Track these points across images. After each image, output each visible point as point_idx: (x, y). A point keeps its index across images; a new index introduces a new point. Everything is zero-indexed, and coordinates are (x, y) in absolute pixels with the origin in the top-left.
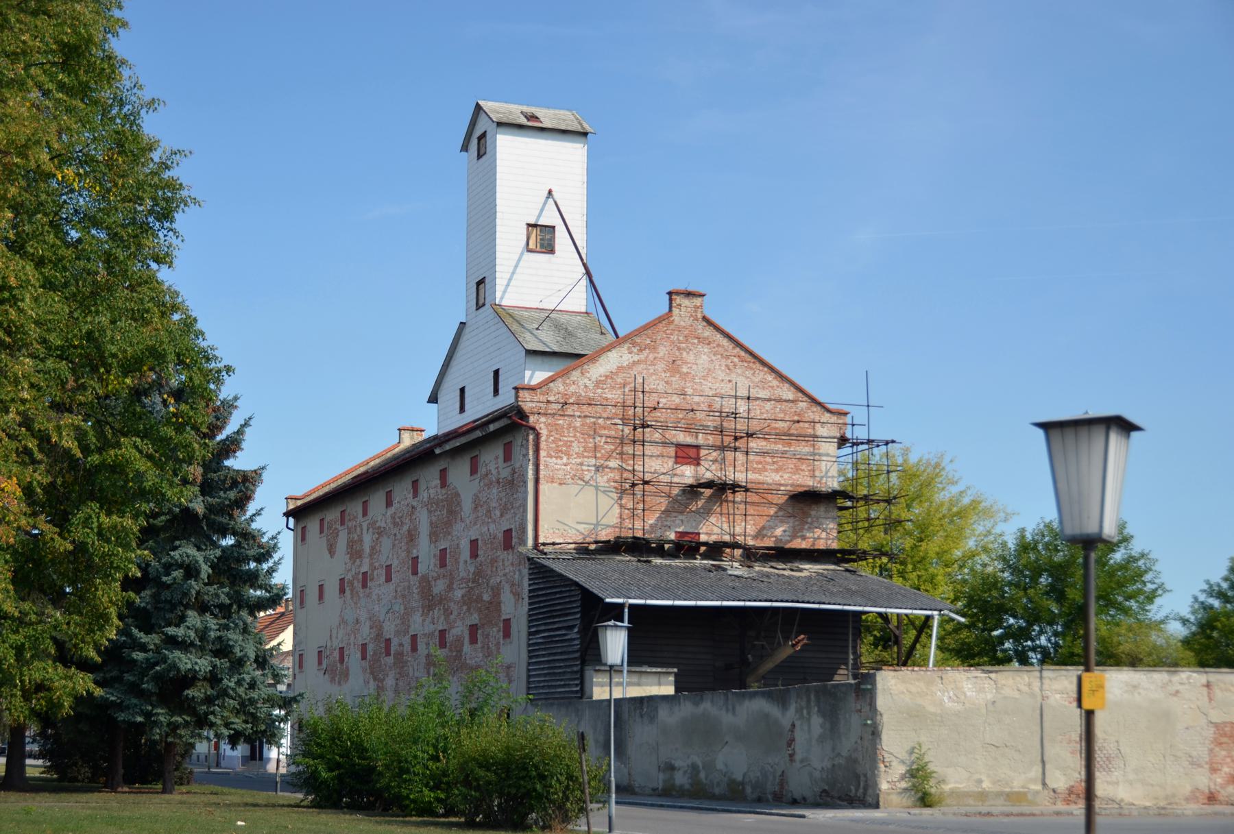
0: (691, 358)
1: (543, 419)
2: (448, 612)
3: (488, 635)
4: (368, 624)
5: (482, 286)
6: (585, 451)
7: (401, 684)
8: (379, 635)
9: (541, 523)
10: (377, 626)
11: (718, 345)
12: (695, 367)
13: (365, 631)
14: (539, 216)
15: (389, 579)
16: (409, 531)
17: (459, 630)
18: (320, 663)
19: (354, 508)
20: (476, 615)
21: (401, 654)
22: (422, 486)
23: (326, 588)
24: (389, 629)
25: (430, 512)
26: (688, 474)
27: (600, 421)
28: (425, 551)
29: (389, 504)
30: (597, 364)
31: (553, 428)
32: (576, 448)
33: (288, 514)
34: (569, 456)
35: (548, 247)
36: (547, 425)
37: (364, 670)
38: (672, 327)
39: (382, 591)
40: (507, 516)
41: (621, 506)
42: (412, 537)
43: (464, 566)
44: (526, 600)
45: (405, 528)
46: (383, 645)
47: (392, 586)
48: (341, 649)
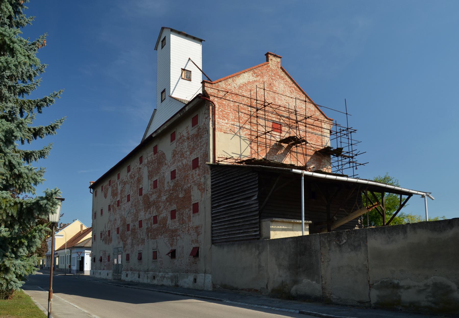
0: (276, 84)
1: (216, 99)
2: (158, 208)
3: (182, 214)
4: (120, 220)
5: (164, 94)
6: (235, 118)
7: (134, 241)
8: (124, 224)
9: (217, 151)
10: (123, 220)
11: (287, 81)
12: (278, 89)
13: (119, 223)
14: (186, 67)
15: (129, 200)
16: (138, 179)
17: (165, 214)
18: (101, 237)
19: (114, 178)
20: (175, 206)
21: (135, 229)
22: (144, 157)
23: (103, 211)
24: (129, 220)
25: (148, 167)
26: (277, 137)
27: (241, 105)
28: (146, 185)
29: (129, 171)
30: (239, 78)
31: (221, 104)
32: (231, 116)
33: (91, 187)
34: (228, 120)
35: (189, 79)
36: (218, 103)
37: (118, 238)
38: (269, 68)
39: (126, 206)
40: (195, 153)
41: (251, 148)
42: (139, 181)
43: (168, 183)
44: (210, 190)
45: (136, 178)
46: (126, 227)
47: (130, 203)
48: (109, 231)
